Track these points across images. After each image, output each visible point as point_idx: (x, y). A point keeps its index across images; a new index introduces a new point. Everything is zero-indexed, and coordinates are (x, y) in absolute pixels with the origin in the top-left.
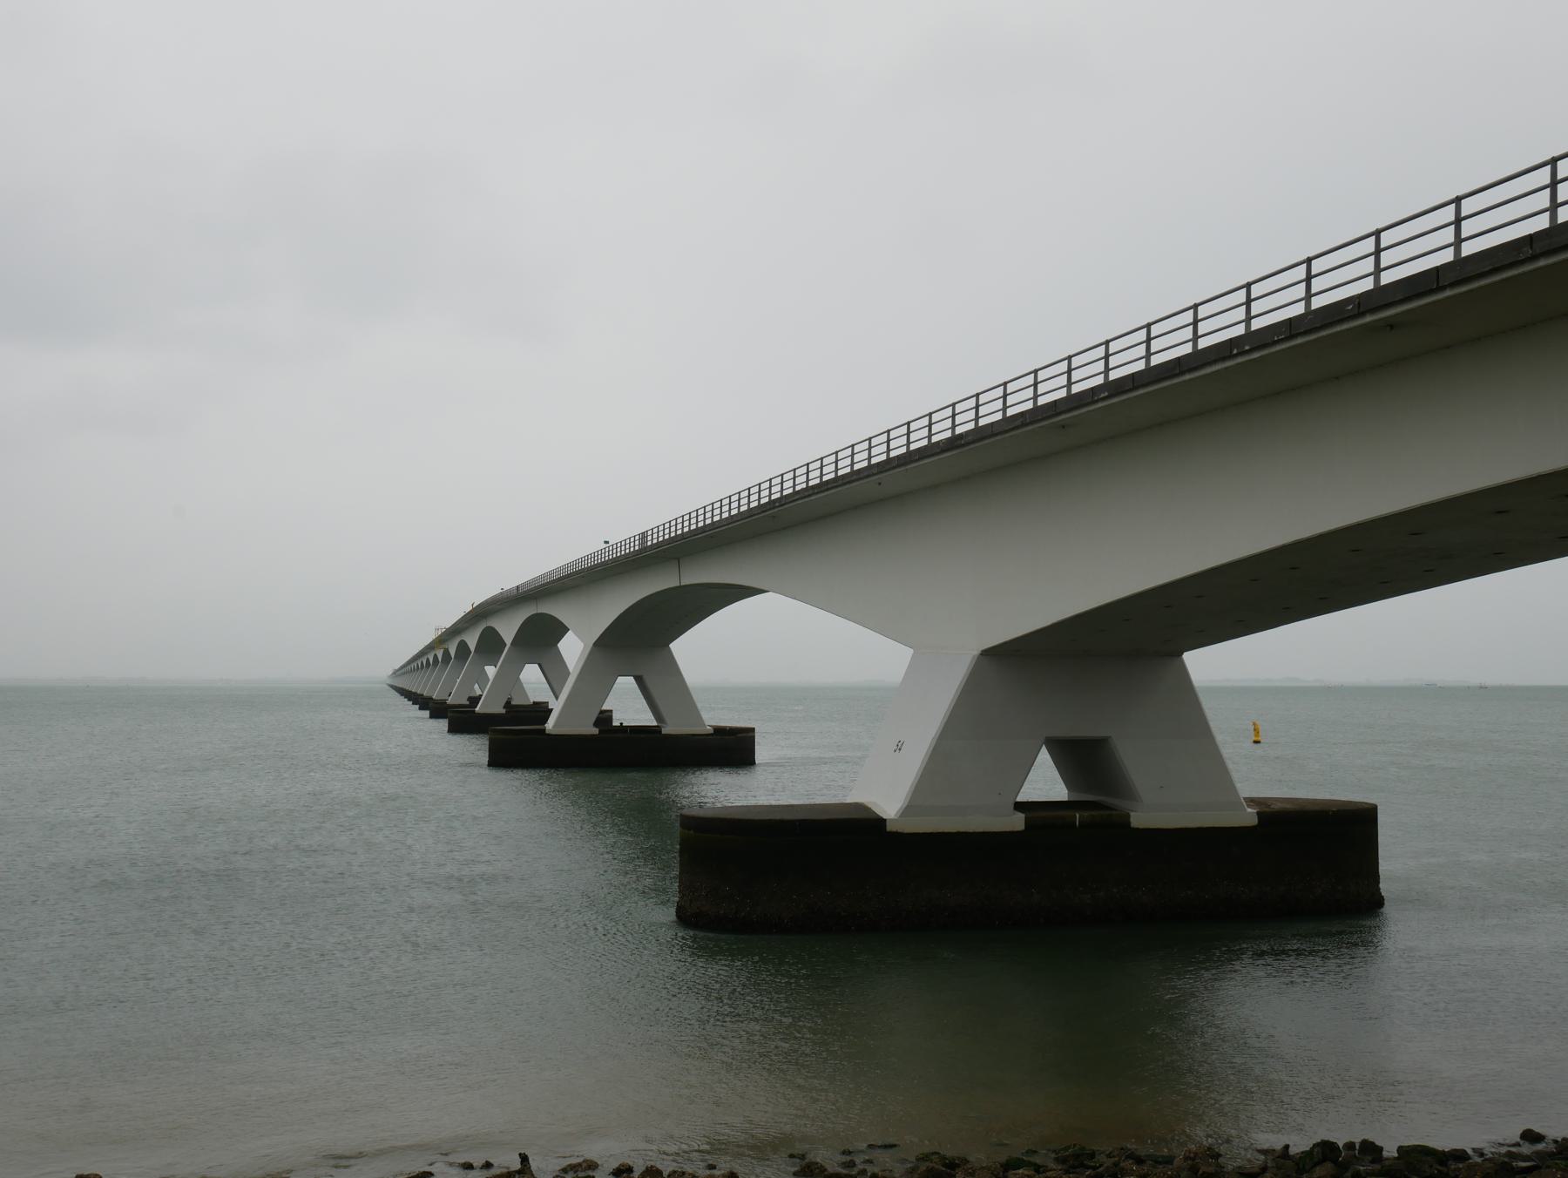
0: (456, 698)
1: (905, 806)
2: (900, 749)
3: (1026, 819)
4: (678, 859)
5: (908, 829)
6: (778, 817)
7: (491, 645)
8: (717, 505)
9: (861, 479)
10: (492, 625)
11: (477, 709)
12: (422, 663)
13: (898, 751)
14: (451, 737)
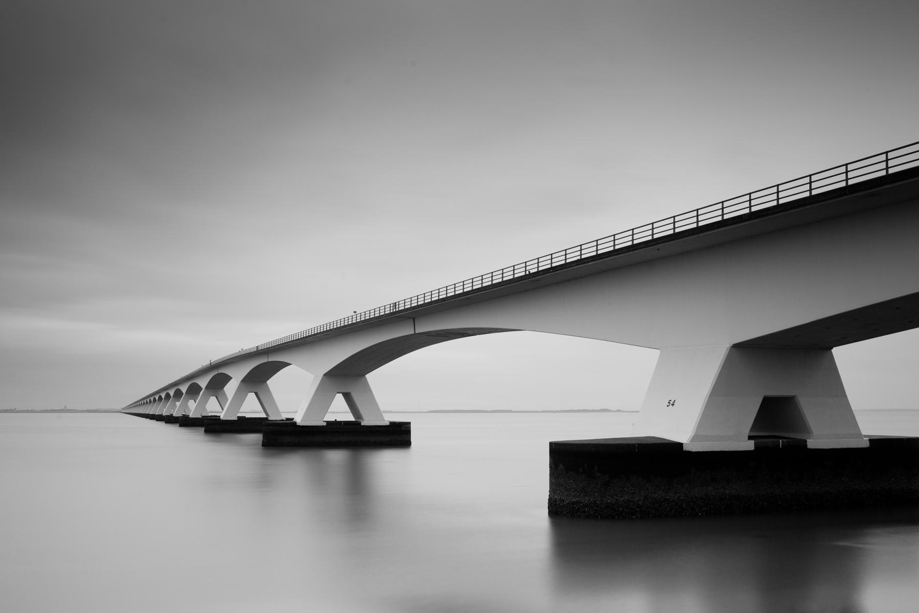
1: (693, 435)
2: (673, 405)
6: (618, 442)
7: (178, 394)
8: (310, 330)
13: (671, 406)
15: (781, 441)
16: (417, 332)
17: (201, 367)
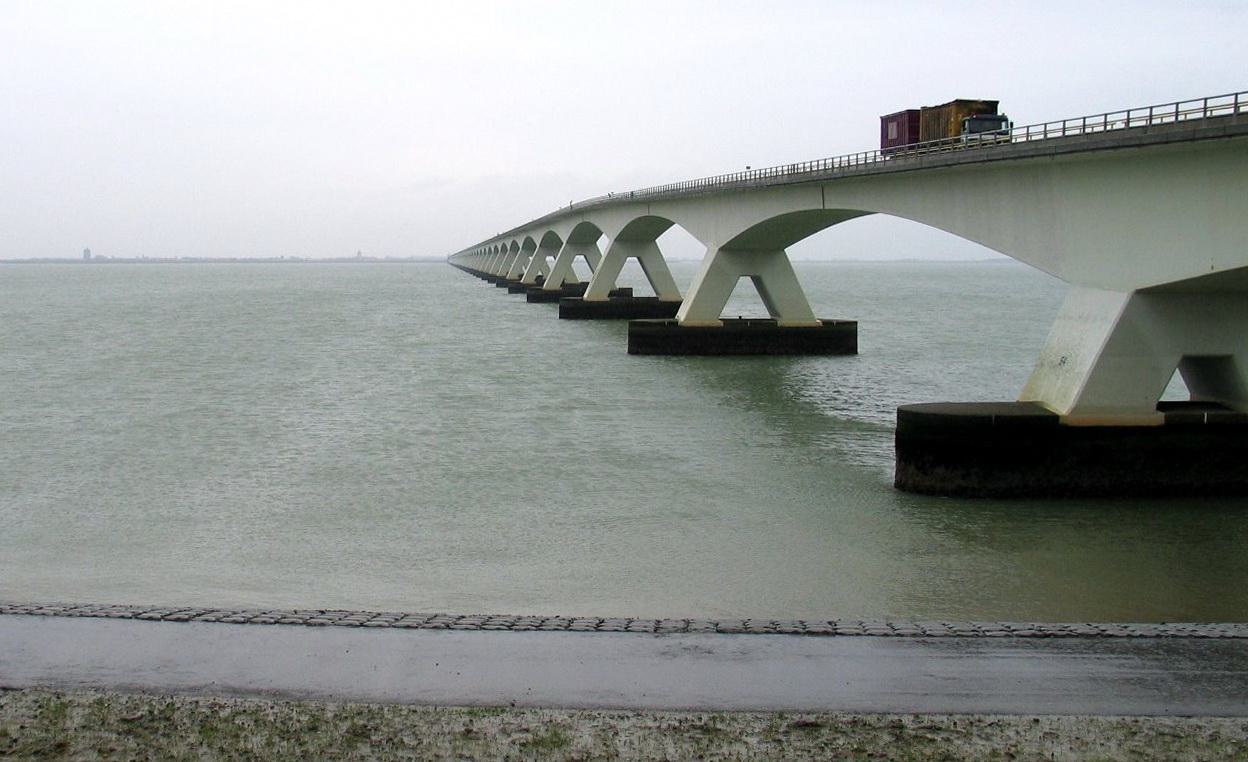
0: (528, 278)
3: (1166, 417)
4: (1213, 625)
5: (689, 325)
7: (529, 245)
9: (975, 162)
10: (592, 222)
11: (585, 296)
12: (490, 249)
14: (637, 360)
15: (1206, 414)
16: (826, 208)
17: (558, 209)
